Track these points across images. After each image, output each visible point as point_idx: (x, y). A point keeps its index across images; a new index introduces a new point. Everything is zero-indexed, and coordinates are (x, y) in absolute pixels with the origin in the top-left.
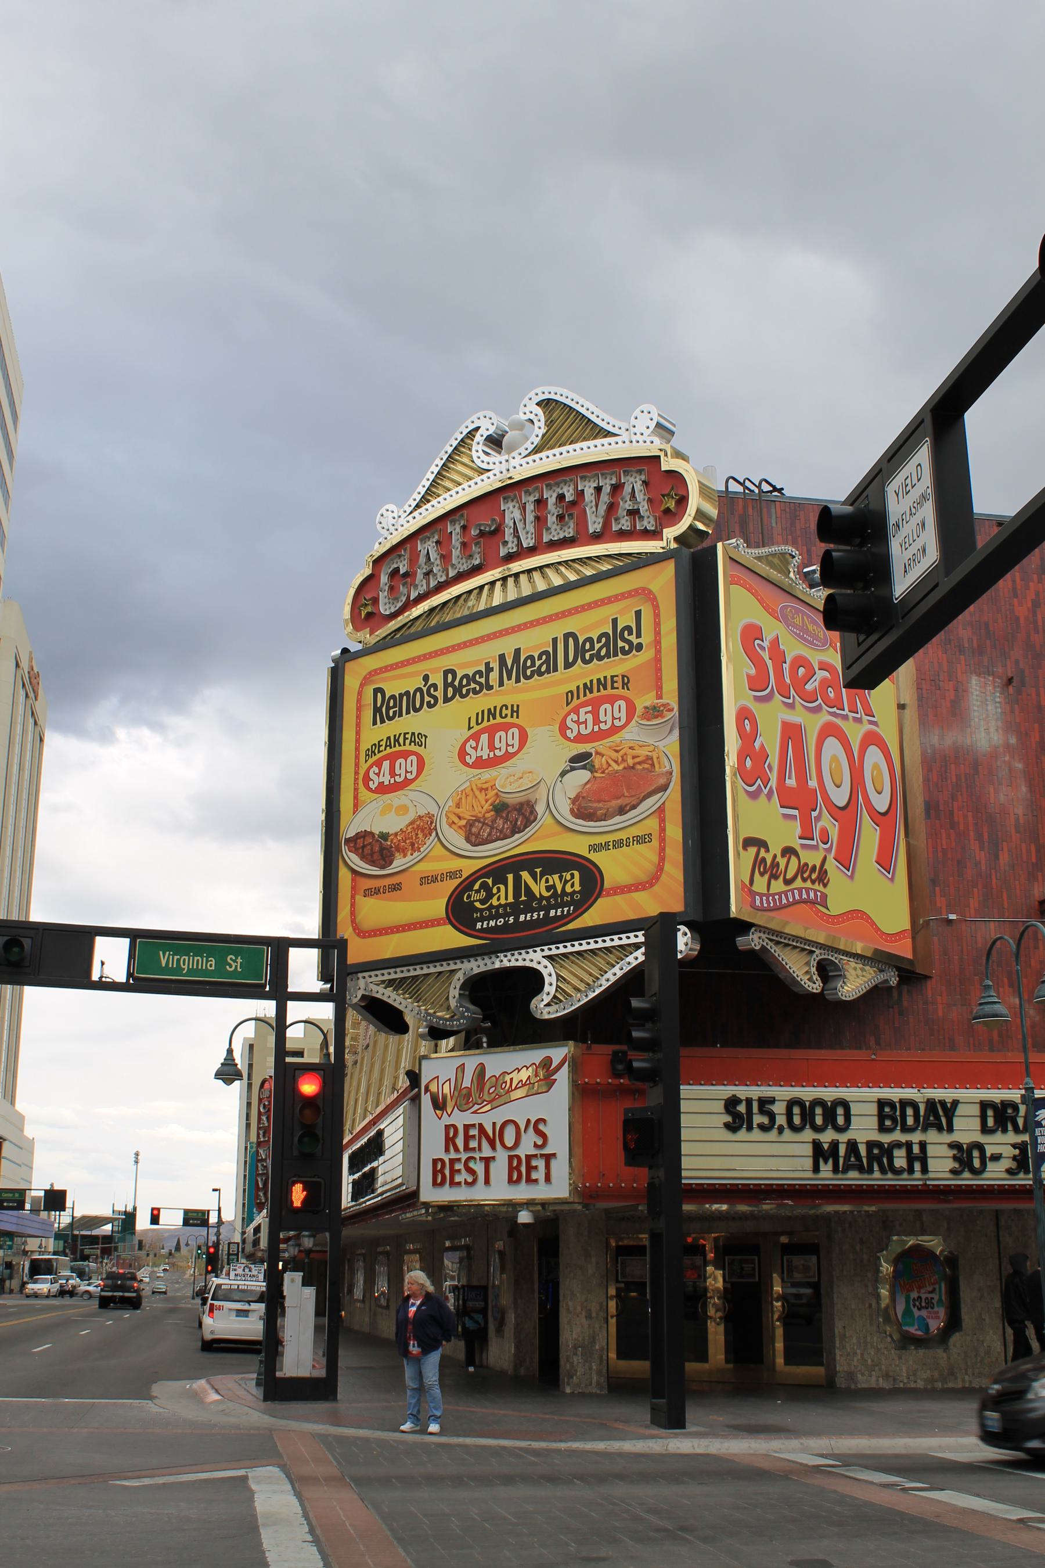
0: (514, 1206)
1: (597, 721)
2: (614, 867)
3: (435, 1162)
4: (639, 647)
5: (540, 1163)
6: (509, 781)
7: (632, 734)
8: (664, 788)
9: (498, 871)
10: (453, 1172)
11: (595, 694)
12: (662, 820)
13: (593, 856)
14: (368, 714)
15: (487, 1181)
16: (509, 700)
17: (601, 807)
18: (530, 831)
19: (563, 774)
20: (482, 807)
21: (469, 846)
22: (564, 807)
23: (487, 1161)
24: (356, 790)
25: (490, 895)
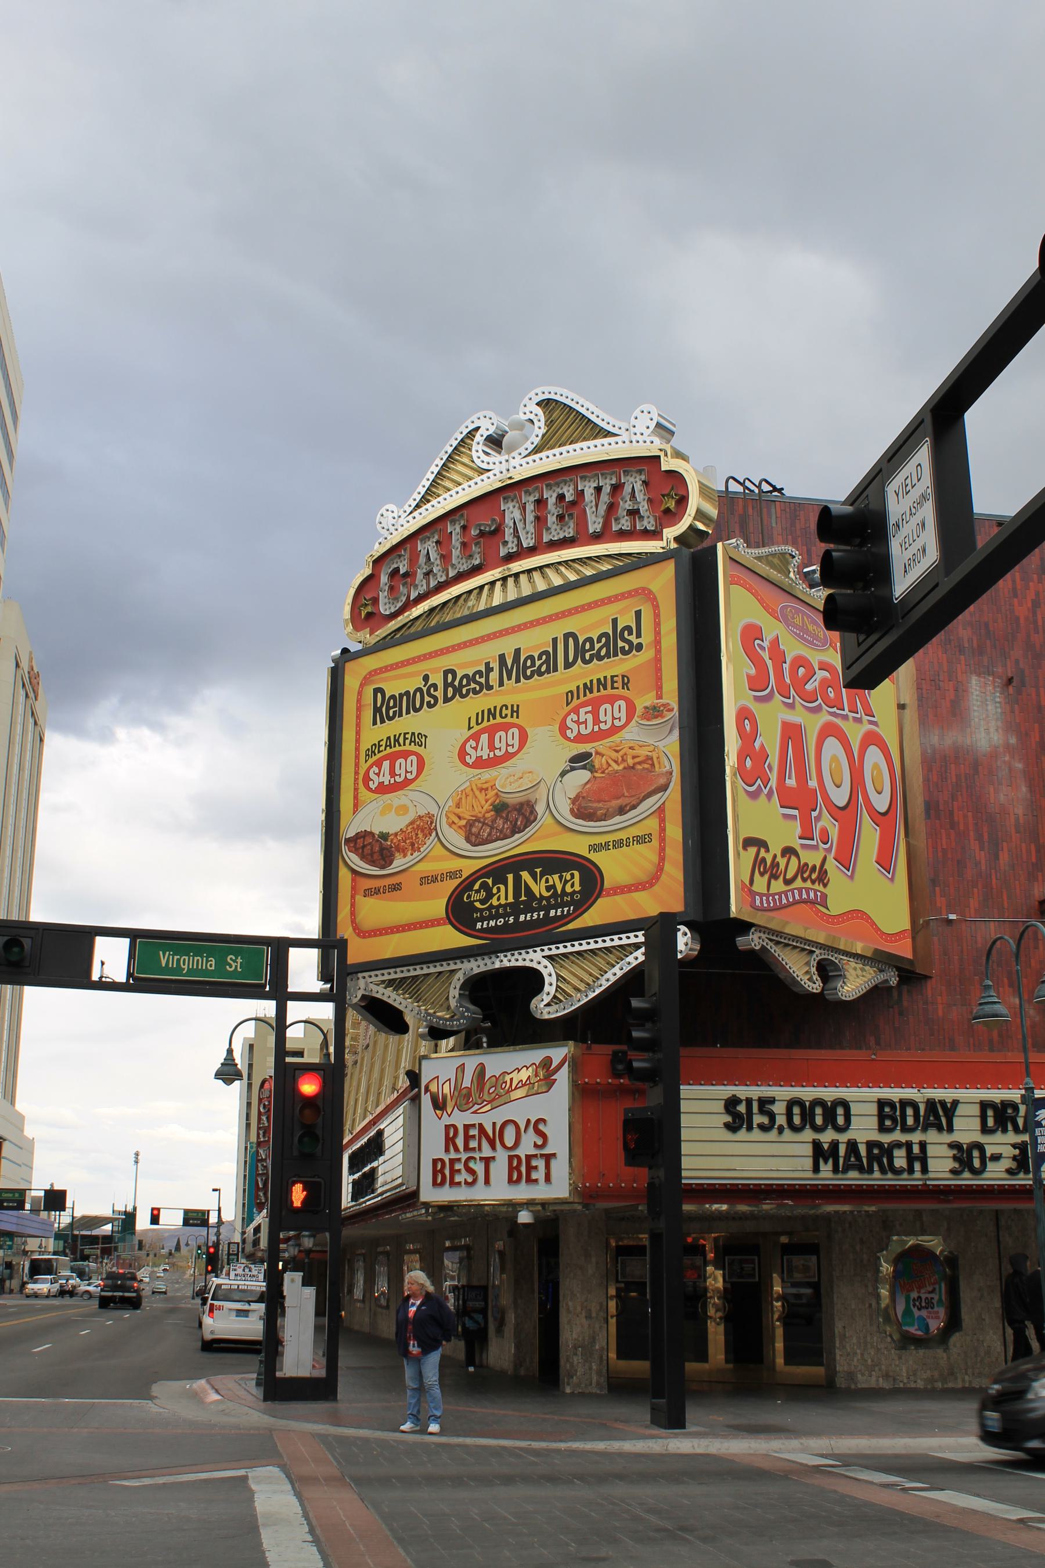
0: (514, 1206)
1: (597, 721)
2: (614, 867)
3: (435, 1162)
4: (639, 647)
5: (540, 1163)
6: (509, 781)
7: (632, 734)
8: (664, 788)
9: (498, 871)
10: (453, 1172)
11: (595, 694)
12: (662, 820)
13: (593, 856)
14: (368, 714)
15: (487, 1181)
16: (509, 700)
17: (601, 807)
18: (530, 831)
19: (563, 774)
20: (482, 807)
21: (469, 846)
22: (564, 807)
23: (487, 1161)
24: (356, 790)
25: (490, 895)
